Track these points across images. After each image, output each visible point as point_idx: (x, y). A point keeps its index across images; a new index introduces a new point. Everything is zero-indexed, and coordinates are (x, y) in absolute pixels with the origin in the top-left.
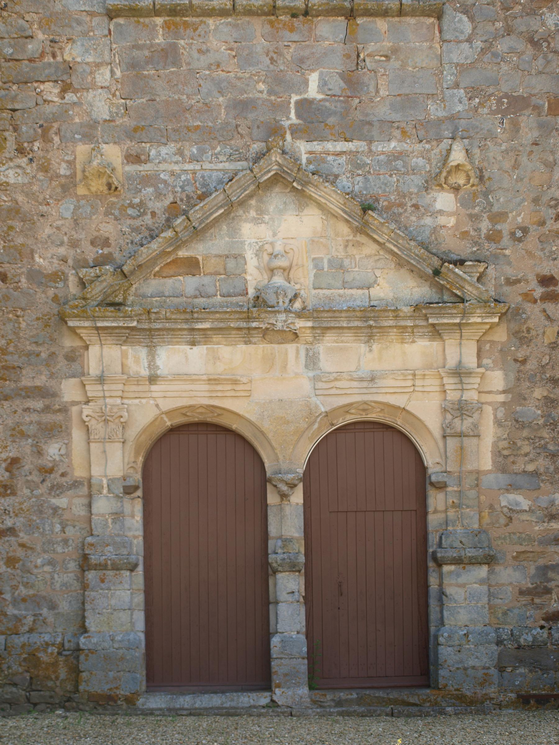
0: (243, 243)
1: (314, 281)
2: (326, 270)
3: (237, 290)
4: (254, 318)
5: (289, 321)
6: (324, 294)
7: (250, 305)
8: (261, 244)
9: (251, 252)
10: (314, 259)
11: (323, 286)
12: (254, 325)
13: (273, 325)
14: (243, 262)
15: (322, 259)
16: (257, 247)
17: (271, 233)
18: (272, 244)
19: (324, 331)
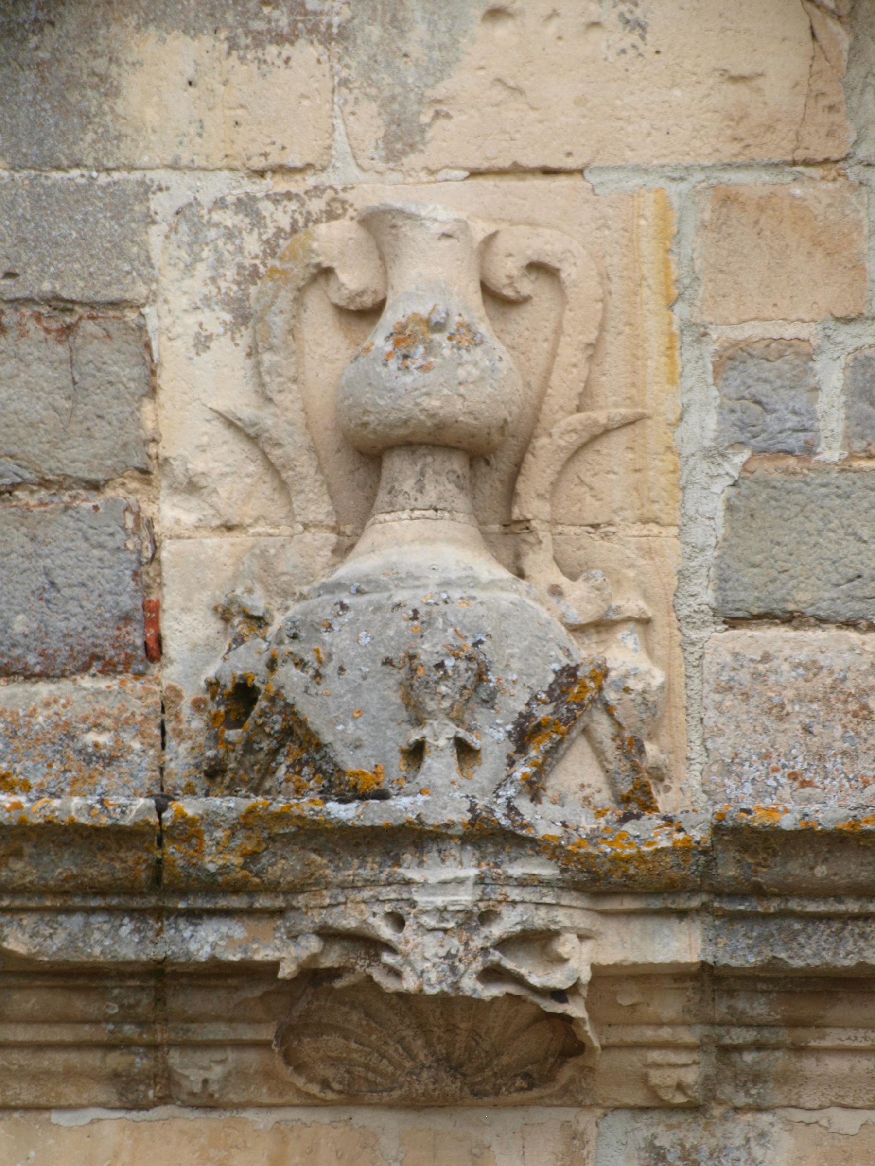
0: (129, 206)
1: (726, 545)
2: (831, 453)
3: (76, 619)
4: (212, 886)
5: (509, 922)
6: (812, 668)
7: (180, 759)
8: (280, 217)
9: (197, 284)
10: (731, 359)
11: (802, 598)
12: (207, 941)
13: (373, 945)
14: (128, 372)
15: (804, 354)
16: (252, 245)
17: (367, 124)
18: (380, 227)
19: (806, 1009)
